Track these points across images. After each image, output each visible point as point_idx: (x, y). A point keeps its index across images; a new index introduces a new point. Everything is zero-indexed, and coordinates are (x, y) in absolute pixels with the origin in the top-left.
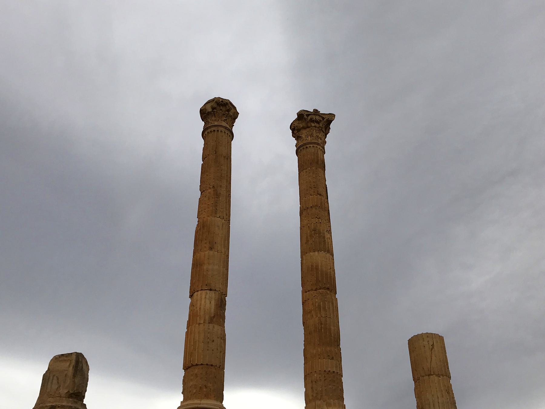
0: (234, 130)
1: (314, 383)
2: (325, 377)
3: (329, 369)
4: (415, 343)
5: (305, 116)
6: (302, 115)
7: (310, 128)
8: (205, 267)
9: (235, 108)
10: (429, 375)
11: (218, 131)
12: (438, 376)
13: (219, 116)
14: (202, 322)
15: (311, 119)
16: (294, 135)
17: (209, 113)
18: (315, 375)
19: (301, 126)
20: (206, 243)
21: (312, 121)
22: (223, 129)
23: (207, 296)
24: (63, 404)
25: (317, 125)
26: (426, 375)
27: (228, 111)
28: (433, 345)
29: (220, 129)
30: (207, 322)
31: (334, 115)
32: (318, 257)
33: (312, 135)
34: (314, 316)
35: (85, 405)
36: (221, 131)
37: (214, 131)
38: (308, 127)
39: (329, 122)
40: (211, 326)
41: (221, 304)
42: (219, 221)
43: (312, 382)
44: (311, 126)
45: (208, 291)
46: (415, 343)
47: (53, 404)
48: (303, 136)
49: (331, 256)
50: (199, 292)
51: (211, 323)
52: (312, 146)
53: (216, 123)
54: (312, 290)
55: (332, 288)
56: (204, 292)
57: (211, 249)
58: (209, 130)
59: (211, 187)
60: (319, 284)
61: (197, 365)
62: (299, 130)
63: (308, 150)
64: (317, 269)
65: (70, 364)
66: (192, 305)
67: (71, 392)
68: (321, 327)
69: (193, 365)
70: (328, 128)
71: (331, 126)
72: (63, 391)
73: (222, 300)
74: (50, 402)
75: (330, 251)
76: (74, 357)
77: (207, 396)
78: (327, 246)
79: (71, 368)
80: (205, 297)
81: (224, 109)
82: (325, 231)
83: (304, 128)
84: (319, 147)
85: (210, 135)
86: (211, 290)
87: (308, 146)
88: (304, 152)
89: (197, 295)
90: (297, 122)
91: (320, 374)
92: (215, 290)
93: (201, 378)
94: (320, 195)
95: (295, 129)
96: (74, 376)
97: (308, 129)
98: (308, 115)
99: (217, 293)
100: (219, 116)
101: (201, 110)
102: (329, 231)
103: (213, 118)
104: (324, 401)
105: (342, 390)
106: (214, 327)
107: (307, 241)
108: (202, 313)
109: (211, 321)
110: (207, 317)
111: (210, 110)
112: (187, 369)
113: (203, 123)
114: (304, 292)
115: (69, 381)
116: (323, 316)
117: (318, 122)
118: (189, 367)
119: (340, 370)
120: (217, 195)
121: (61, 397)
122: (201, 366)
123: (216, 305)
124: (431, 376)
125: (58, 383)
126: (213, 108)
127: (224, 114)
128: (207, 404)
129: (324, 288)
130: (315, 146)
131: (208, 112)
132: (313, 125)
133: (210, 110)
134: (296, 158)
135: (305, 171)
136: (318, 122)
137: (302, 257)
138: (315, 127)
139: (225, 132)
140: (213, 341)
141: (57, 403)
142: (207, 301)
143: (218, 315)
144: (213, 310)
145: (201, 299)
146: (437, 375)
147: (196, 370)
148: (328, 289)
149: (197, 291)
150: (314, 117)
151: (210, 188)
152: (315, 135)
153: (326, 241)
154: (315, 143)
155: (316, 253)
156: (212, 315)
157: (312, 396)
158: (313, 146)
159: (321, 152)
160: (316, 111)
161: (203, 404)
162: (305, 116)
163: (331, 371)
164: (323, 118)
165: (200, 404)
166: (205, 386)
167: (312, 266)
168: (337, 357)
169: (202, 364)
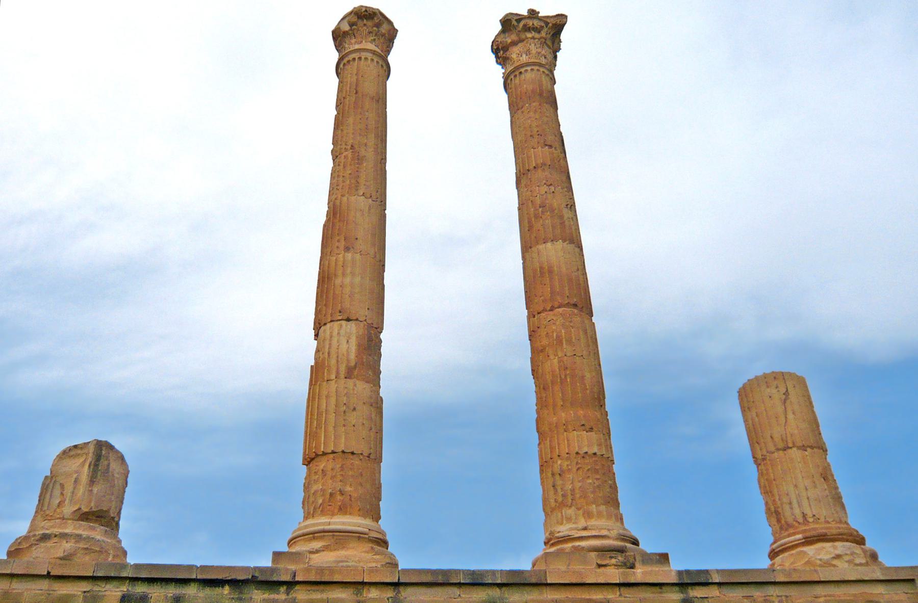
0: (391, 59)
1: (557, 477)
2: (577, 463)
3: (585, 449)
5: (514, 23)
7: (528, 46)
8: (338, 281)
9: (390, 23)
10: (786, 448)
11: (360, 58)
12: (803, 448)
13: (365, 39)
14: (333, 377)
15: (525, 25)
18: (559, 462)
19: (509, 41)
20: (338, 241)
22: (369, 55)
23: (342, 332)
24: (67, 531)
25: (537, 35)
26: (778, 450)
27: (378, 25)
28: (786, 393)
30: (342, 375)
31: (566, 17)
32: (552, 252)
33: (528, 52)
34: (552, 357)
36: (366, 59)
37: (354, 59)
38: (522, 41)
40: (350, 383)
43: (553, 475)
44: (527, 38)
45: (344, 323)
47: (47, 532)
48: (514, 56)
49: (577, 250)
50: (328, 325)
51: (350, 378)
52: (529, 68)
53: (357, 47)
54: (545, 310)
56: (336, 324)
58: (345, 61)
59: (349, 147)
61: (324, 454)
62: (506, 48)
63: (523, 76)
64: (550, 271)
65: (85, 461)
67: (85, 509)
68: (566, 376)
69: (317, 455)
70: (556, 41)
71: (564, 36)
73: (370, 339)
74: (43, 528)
76: (91, 448)
78: (568, 231)
79: (86, 467)
80: (338, 333)
81: (370, 23)
82: (564, 205)
83: (514, 43)
84: (542, 69)
85: (347, 67)
86: (348, 320)
87: (522, 70)
89: (325, 331)
90: (502, 36)
91: (568, 459)
92: (357, 320)
93: (333, 477)
94: (550, 146)
95: (500, 50)
96: (92, 481)
97: (520, 45)
98: (519, 21)
99: (362, 324)
100: (365, 39)
101: (333, 32)
103: (353, 41)
104: (579, 509)
106: (355, 385)
107: (531, 228)
108: (333, 362)
110: (343, 369)
112: (309, 463)
113: (337, 54)
115: (81, 490)
116: (568, 354)
118: (312, 459)
119: (607, 450)
121: (63, 519)
122: (332, 456)
123: (359, 345)
124: (789, 451)
125: (62, 494)
126: (351, 25)
127: (370, 33)
128: (343, 523)
129: (568, 305)
130: (536, 68)
131: (344, 32)
132: (529, 35)
134: (505, 96)
135: (520, 112)
136: (538, 30)
137: (524, 258)
138: (533, 38)
139: (372, 60)
140: (354, 409)
141: (56, 530)
142: (346, 338)
144: (353, 356)
145: (331, 337)
146: (799, 448)
148: (575, 305)
149: (325, 324)
150: (530, 23)
151: (346, 150)
152: (534, 52)
153: (567, 223)
154: (534, 64)
155: (549, 245)
156: (353, 364)
157: (556, 501)
158: (532, 70)
159: (548, 79)
160: (533, 13)
161: (335, 523)
162: (514, 23)
163: (591, 452)
164: (547, 24)
165: (329, 524)
166: (340, 491)
167: (541, 268)
169: (333, 452)
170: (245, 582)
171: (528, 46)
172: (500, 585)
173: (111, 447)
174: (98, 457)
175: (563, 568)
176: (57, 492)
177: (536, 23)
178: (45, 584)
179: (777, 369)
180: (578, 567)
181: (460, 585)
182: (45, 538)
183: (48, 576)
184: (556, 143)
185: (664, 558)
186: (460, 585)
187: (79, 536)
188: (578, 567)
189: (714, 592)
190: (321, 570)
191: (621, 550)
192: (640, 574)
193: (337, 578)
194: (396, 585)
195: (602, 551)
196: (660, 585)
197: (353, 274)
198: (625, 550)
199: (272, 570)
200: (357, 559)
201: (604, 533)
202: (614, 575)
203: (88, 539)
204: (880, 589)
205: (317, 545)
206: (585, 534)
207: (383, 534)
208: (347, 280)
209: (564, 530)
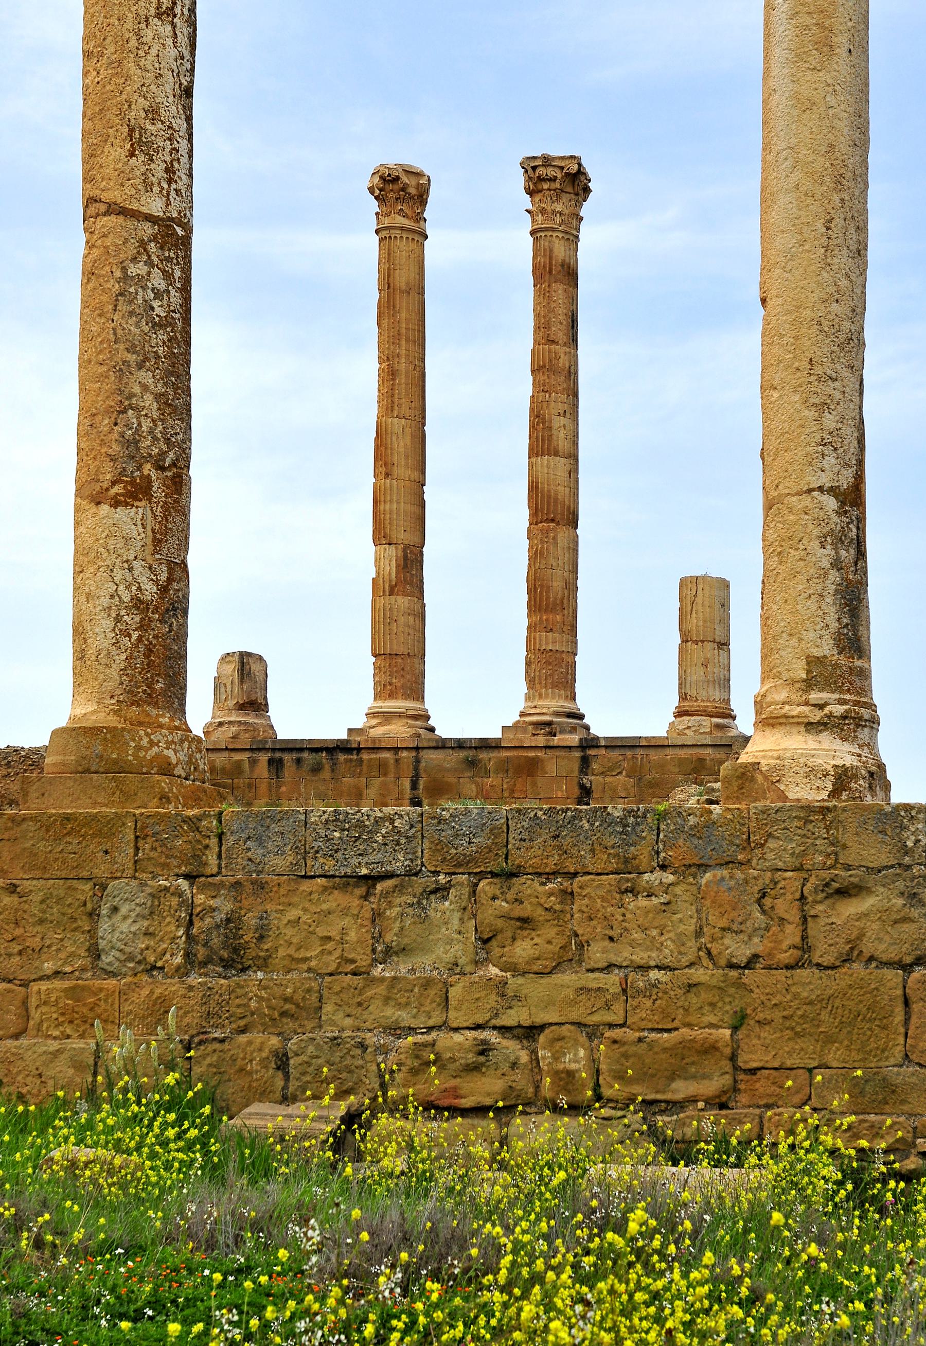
7: (558, 185)
13: (401, 194)
96: (242, 681)
100: (401, 194)
117: (553, 179)
123: (397, 566)
132: (546, 186)
170: (334, 748)
171: (558, 185)
172: (476, 748)
173: (250, 654)
174: (242, 664)
175: (512, 736)
176: (223, 690)
177: (551, 172)
178: (226, 754)
180: (520, 736)
181: (452, 748)
182: (221, 724)
183: (227, 749)
186: (452, 748)
187: (240, 722)
188: (520, 736)
190: (374, 740)
191: (549, 724)
193: (383, 745)
196: (570, 747)
199: (347, 741)
200: (399, 731)
201: (545, 711)
202: (541, 741)
203: (246, 723)
204: (709, 751)
206: (533, 711)
207: (427, 711)
208: (387, 507)
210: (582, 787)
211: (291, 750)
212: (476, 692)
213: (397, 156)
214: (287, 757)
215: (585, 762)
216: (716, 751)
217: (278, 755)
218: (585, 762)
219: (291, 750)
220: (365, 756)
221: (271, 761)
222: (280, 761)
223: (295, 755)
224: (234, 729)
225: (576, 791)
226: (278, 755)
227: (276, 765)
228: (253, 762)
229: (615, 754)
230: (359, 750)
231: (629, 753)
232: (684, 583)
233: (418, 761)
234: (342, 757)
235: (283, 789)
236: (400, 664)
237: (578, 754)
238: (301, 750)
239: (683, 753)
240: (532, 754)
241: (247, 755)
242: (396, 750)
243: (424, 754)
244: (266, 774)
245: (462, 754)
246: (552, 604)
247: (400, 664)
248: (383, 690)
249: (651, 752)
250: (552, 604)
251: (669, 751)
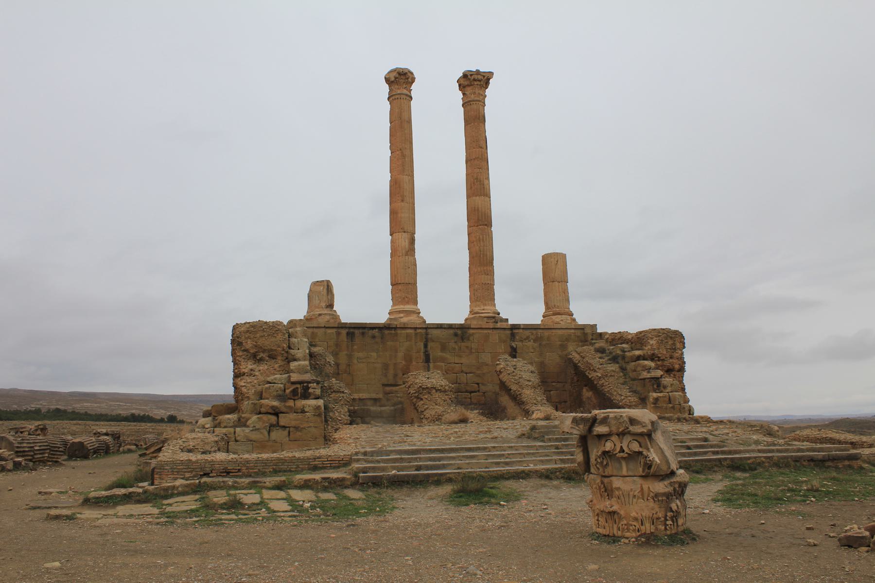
4: (547, 260)
6: (465, 76)
7: (474, 84)
13: (400, 81)
16: (460, 90)
17: (392, 82)
21: (474, 80)
22: (404, 97)
29: (402, 96)
32: (478, 200)
33: (474, 93)
35: (291, 322)
39: (488, 79)
41: (412, 241)
42: (406, 178)
46: (547, 260)
53: (399, 92)
55: (489, 224)
57: (402, 201)
60: (479, 221)
62: (464, 87)
66: (392, 242)
72: (323, 305)
75: (488, 196)
77: (408, 303)
83: (468, 86)
88: (469, 107)
100: (400, 81)
102: (488, 178)
105: (494, 295)
109: (407, 254)
111: (393, 79)
114: (469, 226)
117: (480, 81)
120: (404, 156)
126: (396, 78)
133: (393, 79)
136: (480, 81)
143: (411, 250)
145: (131, 516)
147: (400, 287)
150: (476, 77)
168: (491, 273)
171: (474, 84)
177: (480, 77)
178: (323, 330)
179: (687, 367)
184: (413, 267)
185: (507, 320)
189: (521, 331)
190: (404, 324)
191: (494, 317)
192: (499, 325)
194: (426, 328)
195: (488, 317)
197: (49, 454)
198: (496, 318)
202: (491, 325)
204: (573, 331)
205: (402, 315)
209: (476, 309)
210: (512, 347)
211: (359, 328)
212: (444, 302)
213: (402, 65)
214: (357, 332)
215: (513, 335)
216: (576, 331)
217: (352, 330)
218: (513, 335)
219: (359, 328)
220: (399, 331)
221: (348, 334)
222: (353, 334)
223: (361, 331)
224: (328, 317)
225: (509, 350)
226: (352, 330)
227: (351, 335)
228: (338, 334)
229: (527, 333)
230: (396, 328)
231: (534, 332)
232: (673, 340)
233: (427, 334)
234: (387, 332)
235: (355, 347)
236: (404, 285)
237: (509, 332)
238: (364, 328)
239: (560, 332)
240: (486, 331)
241: (335, 330)
242: (416, 329)
243: (429, 331)
244: (345, 340)
245: (452, 331)
246: (481, 260)
247: (404, 285)
248: (395, 300)
249: (545, 331)
250: (481, 260)
251: (554, 331)
